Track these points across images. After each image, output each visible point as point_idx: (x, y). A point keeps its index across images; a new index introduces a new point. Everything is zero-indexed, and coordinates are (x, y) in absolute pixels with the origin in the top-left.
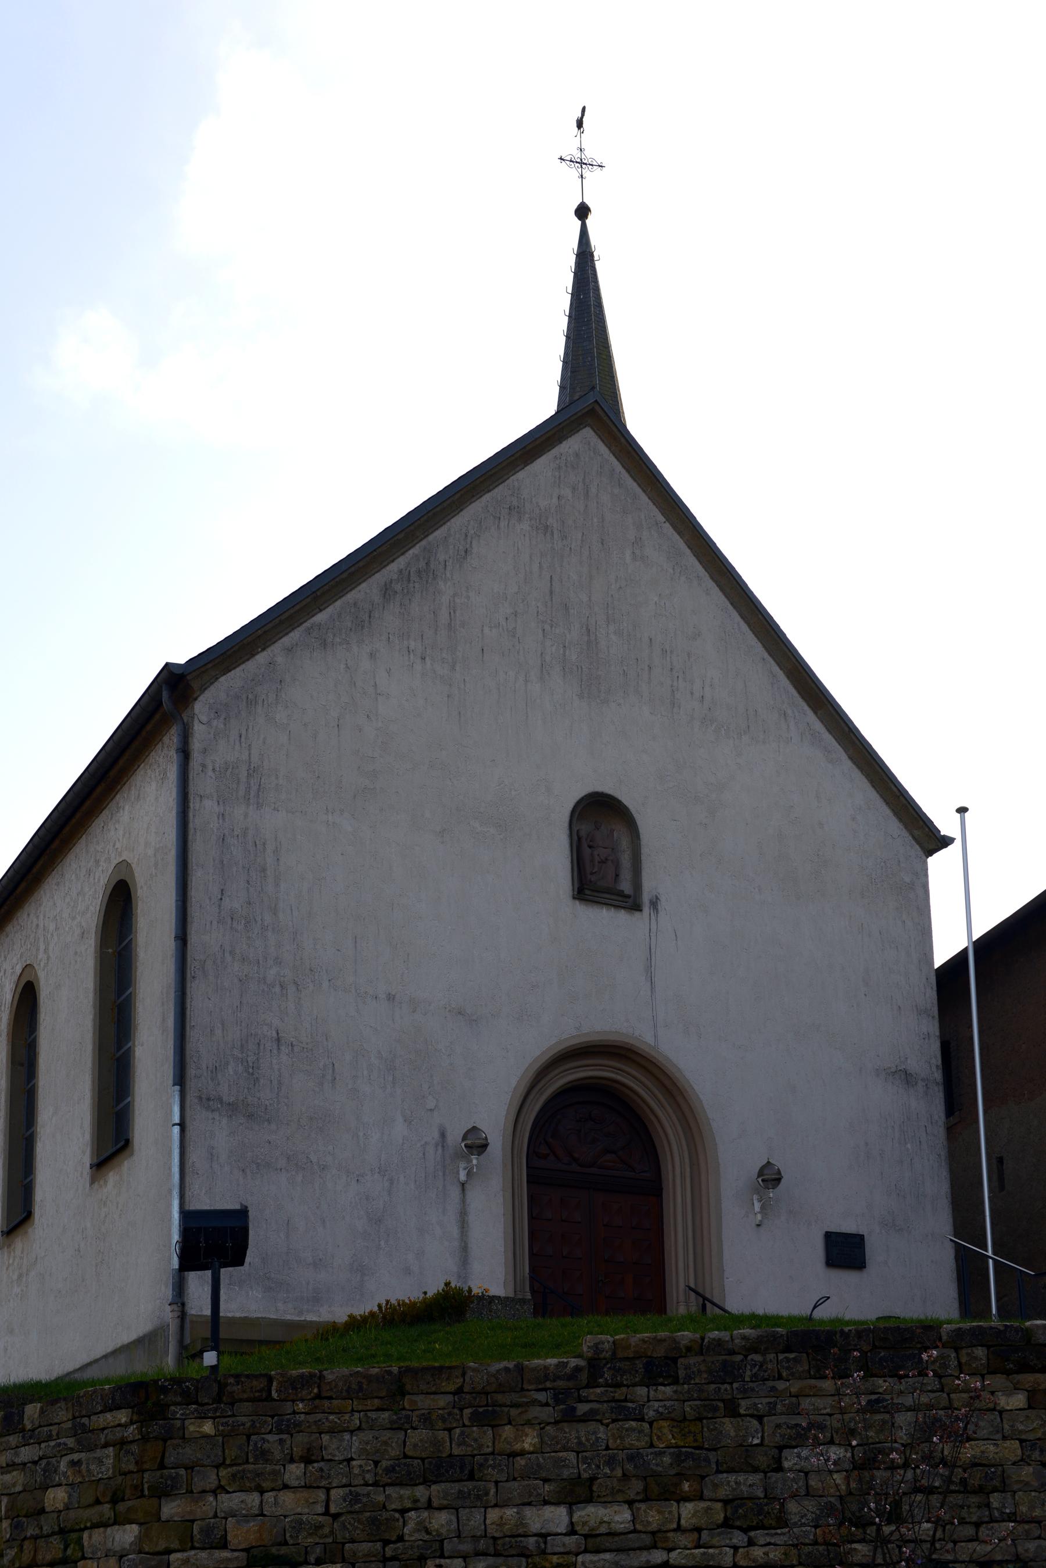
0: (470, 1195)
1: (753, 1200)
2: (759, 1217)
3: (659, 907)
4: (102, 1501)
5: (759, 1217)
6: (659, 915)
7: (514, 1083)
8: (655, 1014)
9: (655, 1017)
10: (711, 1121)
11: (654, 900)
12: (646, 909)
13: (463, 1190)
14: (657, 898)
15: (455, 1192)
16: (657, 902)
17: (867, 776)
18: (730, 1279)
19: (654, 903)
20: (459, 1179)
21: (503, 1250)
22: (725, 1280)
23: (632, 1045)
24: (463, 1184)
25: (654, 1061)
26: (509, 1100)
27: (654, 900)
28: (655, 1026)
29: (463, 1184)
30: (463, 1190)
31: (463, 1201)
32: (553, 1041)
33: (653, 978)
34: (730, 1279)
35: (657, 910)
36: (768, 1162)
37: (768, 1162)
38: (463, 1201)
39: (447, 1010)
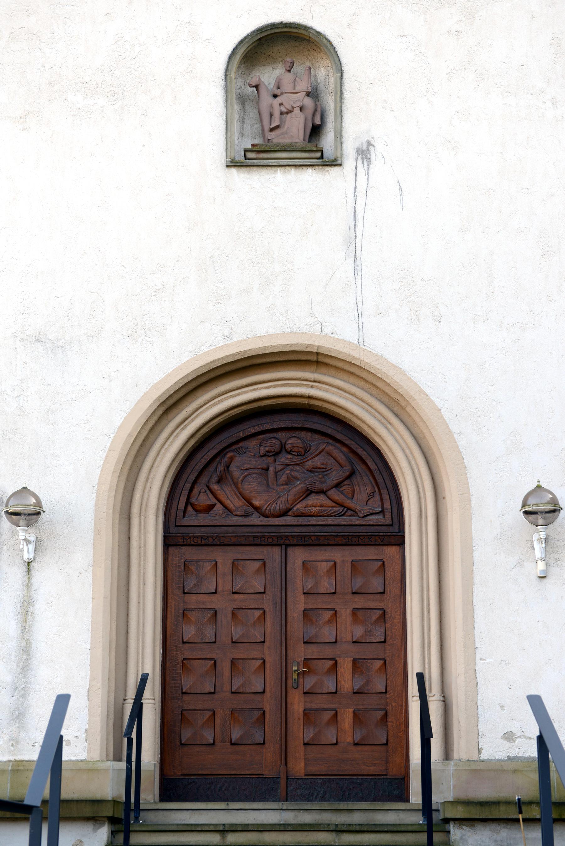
0: (38, 576)
1: (532, 541)
2: (541, 565)
3: (373, 157)
4: (271, 487)
5: (541, 565)
6: (371, 166)
7: (118, 420)
8: (359, 298)
9: (360, 305)
10: (455, 436)
11: (365, 148)
12: (349, 162)
13: (29, 571)
14: (369, 144)
15: (19, 571)
16: (368, 150)
17: (164, 530)
18: (488, 661)
19: (363, 152)
20: (22, 557)
21: (89, 646)
22: (478, 661)
23: (318, 347)
24: (29, 564)
25: (358, 364)
26: (108, 445)
27: (365, 148)
28: (359, 316)
29: (29, 564)
30: (29, 571)
31: (28, 586)
32: (185, 358)
33: (358, 253)
34: (488, 661)
35: (369, 160)
36: (539, 487)
37: (539, 487)
38: (28, 586)
39: (19, 339)
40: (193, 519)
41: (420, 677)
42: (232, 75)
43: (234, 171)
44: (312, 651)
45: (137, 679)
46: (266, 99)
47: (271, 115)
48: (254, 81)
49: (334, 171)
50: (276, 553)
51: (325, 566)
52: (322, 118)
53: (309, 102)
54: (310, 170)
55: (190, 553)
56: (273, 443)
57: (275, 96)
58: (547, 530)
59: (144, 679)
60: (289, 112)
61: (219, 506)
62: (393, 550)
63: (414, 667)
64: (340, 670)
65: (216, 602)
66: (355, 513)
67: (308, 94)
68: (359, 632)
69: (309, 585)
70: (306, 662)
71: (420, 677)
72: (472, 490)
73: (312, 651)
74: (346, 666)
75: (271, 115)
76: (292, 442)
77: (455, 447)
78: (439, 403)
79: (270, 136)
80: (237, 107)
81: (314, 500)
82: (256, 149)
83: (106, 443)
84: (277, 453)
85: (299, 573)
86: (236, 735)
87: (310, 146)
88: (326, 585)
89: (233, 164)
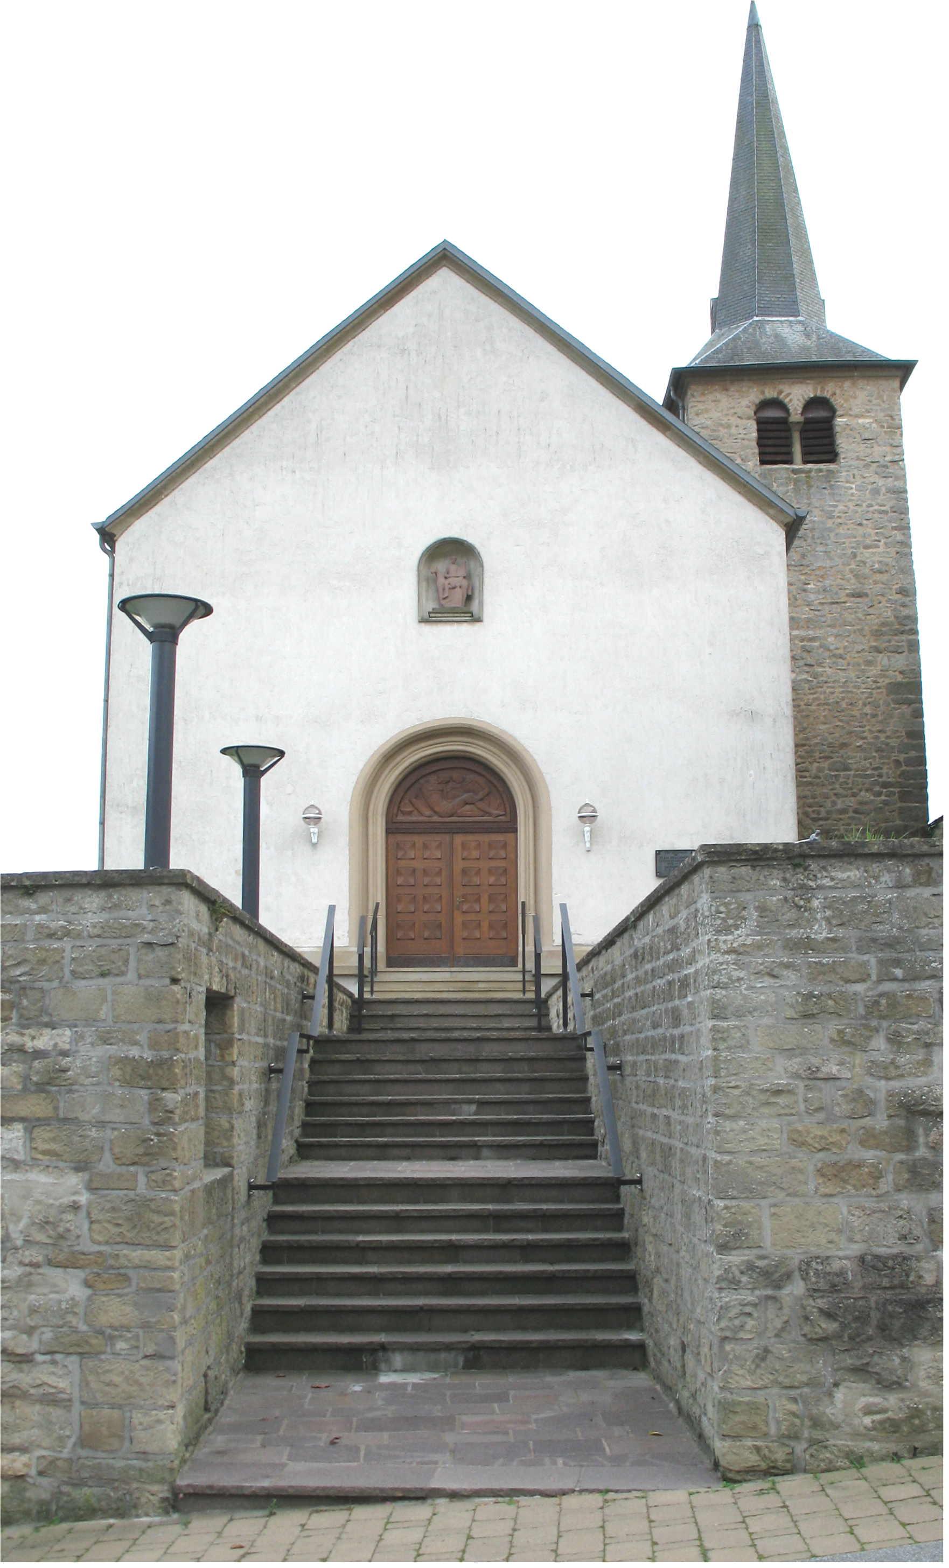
5: (588, 845)
7: (361, 765)
32: (397, 731)
40: (401, 818)
41: (523, 903)
42: (421, 568)
43: (423, 624)
44: (467, 864)
45: (367, 906)
46: (441, 580)
47: (444, 589)
48: (433, 570)
49: (478, 625)
50: (447, 837)
51: (473, 844)
52: (473, 590)
53: (465, 583)
54: (465, 624)
55: (400, 838)
56: (444, 775)
57: (446, 578)
58: (58, 958)
59: (377, 905)
60: (454, 588)
61: (416, 812)
62: (512, 835)
63: (521, 898)
64: (482, 900)
65: (415, 864)
66: (490, 814)
67: (464, 577)
68: (492, 880)
69: (465, 854)
70: (463, 896)
71: (523, 903)
72: (552, 805)
73: (467, 864)
74: (485, 899)
75: (444, 589)
76: (455, 775)
77: (544, 781)
78: (536, 757)
79: (443, 602)
80: (424, 584)
81: (468, 807)
82: (434, 611)
83: (355, 778)
84: (448, 782)
85: (460, 848)
86: (426, 934)
87: (465, 609)
88: (475, 854)
89: (423, 621)
